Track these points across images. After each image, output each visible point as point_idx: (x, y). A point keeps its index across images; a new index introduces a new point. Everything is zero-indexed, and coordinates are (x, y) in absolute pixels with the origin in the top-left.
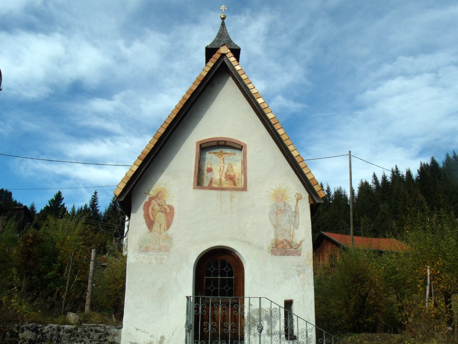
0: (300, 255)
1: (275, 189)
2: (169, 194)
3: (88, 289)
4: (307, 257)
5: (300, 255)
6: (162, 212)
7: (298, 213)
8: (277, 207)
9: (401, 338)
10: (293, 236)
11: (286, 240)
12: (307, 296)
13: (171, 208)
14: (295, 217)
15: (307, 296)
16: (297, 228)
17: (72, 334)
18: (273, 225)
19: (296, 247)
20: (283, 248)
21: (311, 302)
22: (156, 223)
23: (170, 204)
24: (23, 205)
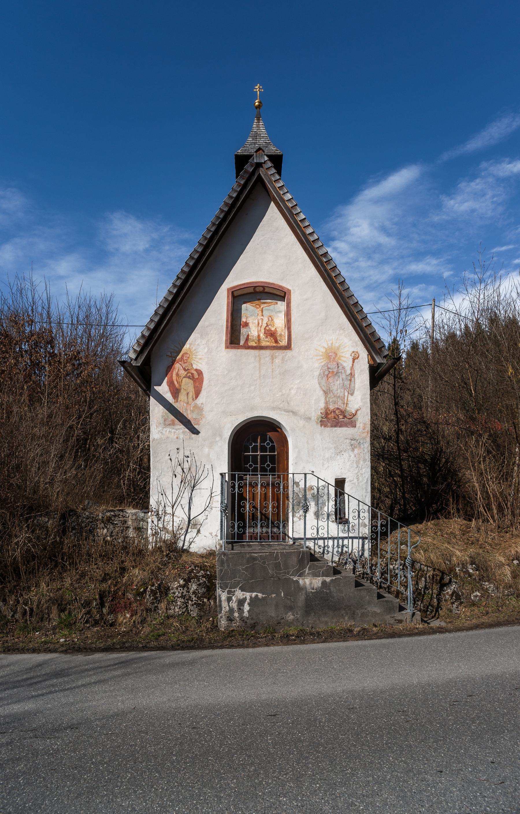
0: (355, 426)
1: (327, 347)
5: (355, 426)
6: (189, 377)
8: (328, 368)
11: (338, 409)
12: (362, 474)
14: (351, 380)
16: (352, 394)
18: (324, 391)
20: (335, 418)
21: (367, 482)
22: (182, 391)
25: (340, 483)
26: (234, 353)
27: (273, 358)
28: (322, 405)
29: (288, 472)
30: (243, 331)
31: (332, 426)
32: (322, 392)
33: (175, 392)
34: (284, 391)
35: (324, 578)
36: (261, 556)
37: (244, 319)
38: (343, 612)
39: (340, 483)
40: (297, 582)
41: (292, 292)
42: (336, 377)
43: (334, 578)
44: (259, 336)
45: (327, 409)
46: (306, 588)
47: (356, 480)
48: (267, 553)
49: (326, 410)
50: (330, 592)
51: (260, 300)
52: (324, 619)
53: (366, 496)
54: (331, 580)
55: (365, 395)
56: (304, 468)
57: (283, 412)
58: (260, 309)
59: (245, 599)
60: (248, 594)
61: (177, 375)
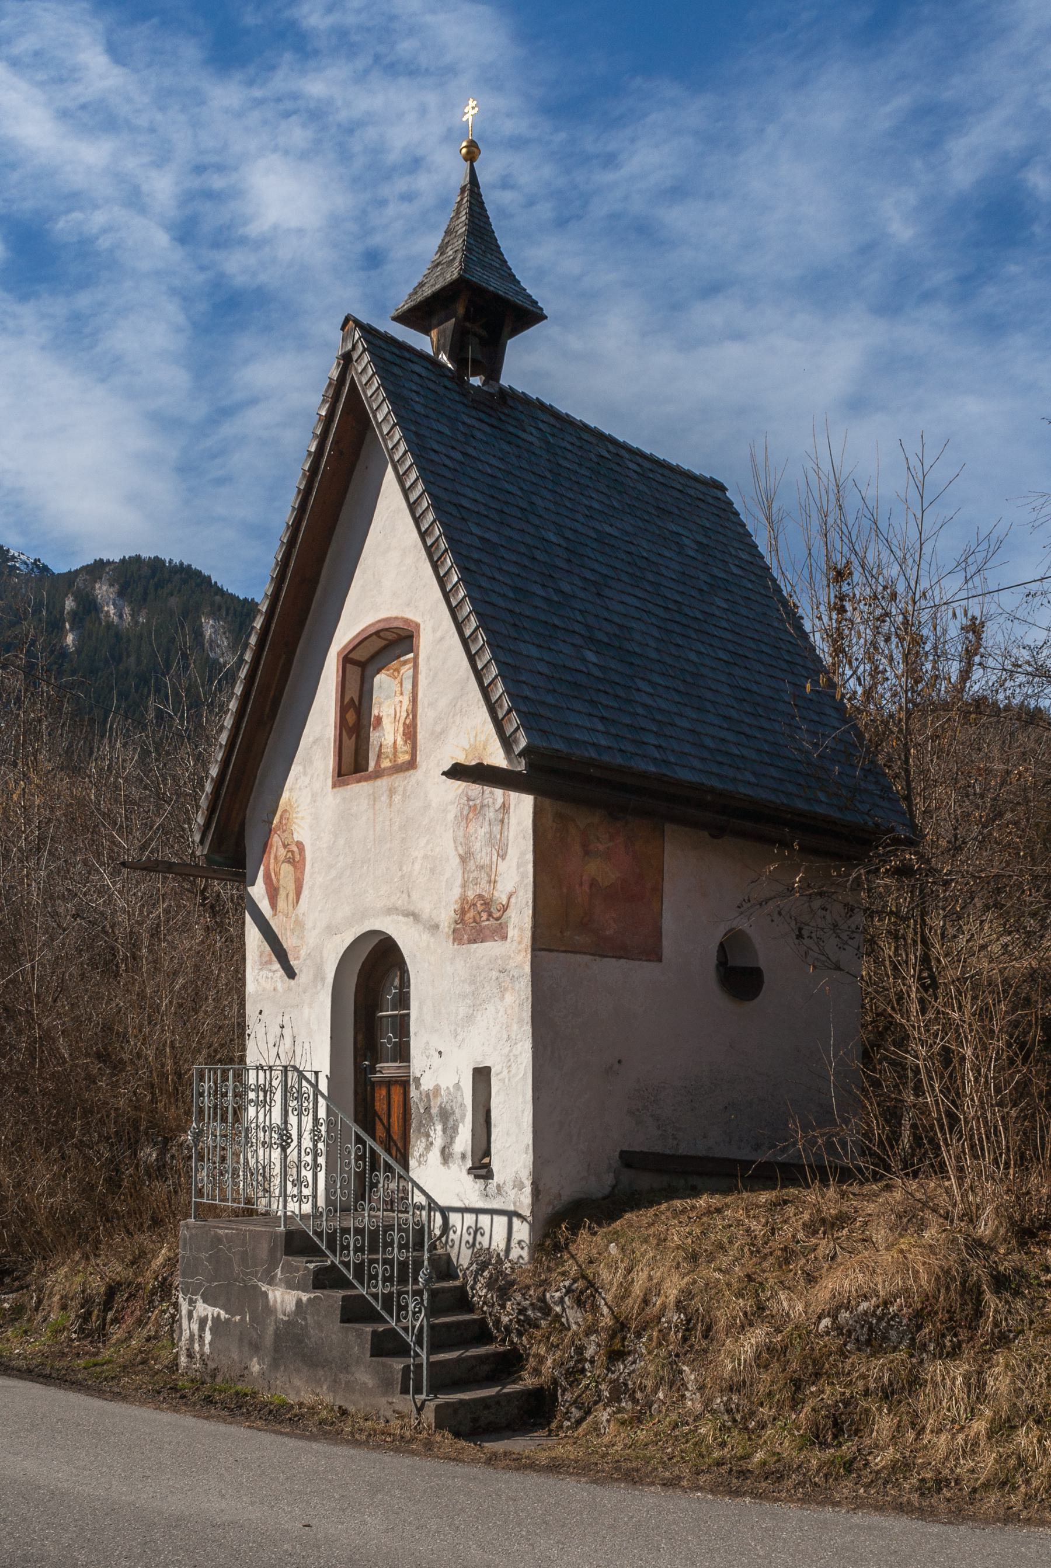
0: (504, 938)
1: (467, 747)
2: (297, 812)
3: (958, 146)
4: (520, 943)
5: (504, 938)
6: (289, 862)
7: (508, 812)
8: (469, 800)
9: (827, 1186)
10: (495, 882)
11: (480, 896)
12: (516, 1056)
13: (300, 846)
14: (502, 821)
15: (516, 1056)
16: (503, 857)
17: (671, 1347)
18: (460, 855)
19: (498, 915)
20: (475, 921)
21: (525, 1073)
22: (281, 889)
23: (300, 839)
24: (117, 560)
25: (482, 1076)
26: (359, 790)
27: (374, 798)
28: (457, 892)
29: (242, 1059)
30: (374, 736)
31: (470, 942)
32: (458, 860)
33: (273, 894)
34: (404, 868)
35: (300, 1293)
36: (227, 1234)
37: (375, 712)
38: (321, 1373)
39: (482, 1076)
40: (265, 1294)
41: (422, 627)
42: (481, 818)
43: (312, 1296)
44: (395, 743)
45: (464, 899)
46: (276, 1310)
47: (505, 1071)
48: (233, 1229)
49: (462, 904)
50: (307, 1324)
51: (399, 657)
52: (297, 1382)
53: (523, 1112)
54: (309, 1299)
55: (523, 854)
56: (428, 1043)
57: (401, 918)
58: (399, 679)
59: (206, 1317)
60: (210, 1309)
61: (276, 858)
